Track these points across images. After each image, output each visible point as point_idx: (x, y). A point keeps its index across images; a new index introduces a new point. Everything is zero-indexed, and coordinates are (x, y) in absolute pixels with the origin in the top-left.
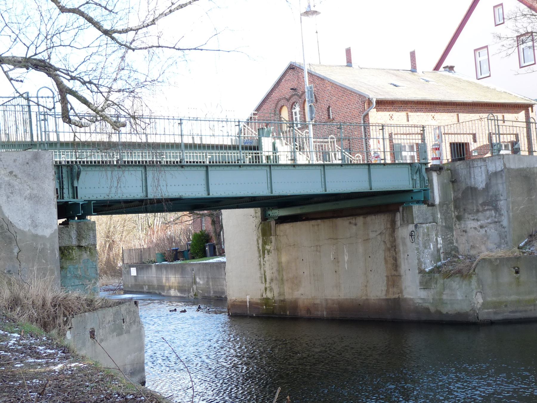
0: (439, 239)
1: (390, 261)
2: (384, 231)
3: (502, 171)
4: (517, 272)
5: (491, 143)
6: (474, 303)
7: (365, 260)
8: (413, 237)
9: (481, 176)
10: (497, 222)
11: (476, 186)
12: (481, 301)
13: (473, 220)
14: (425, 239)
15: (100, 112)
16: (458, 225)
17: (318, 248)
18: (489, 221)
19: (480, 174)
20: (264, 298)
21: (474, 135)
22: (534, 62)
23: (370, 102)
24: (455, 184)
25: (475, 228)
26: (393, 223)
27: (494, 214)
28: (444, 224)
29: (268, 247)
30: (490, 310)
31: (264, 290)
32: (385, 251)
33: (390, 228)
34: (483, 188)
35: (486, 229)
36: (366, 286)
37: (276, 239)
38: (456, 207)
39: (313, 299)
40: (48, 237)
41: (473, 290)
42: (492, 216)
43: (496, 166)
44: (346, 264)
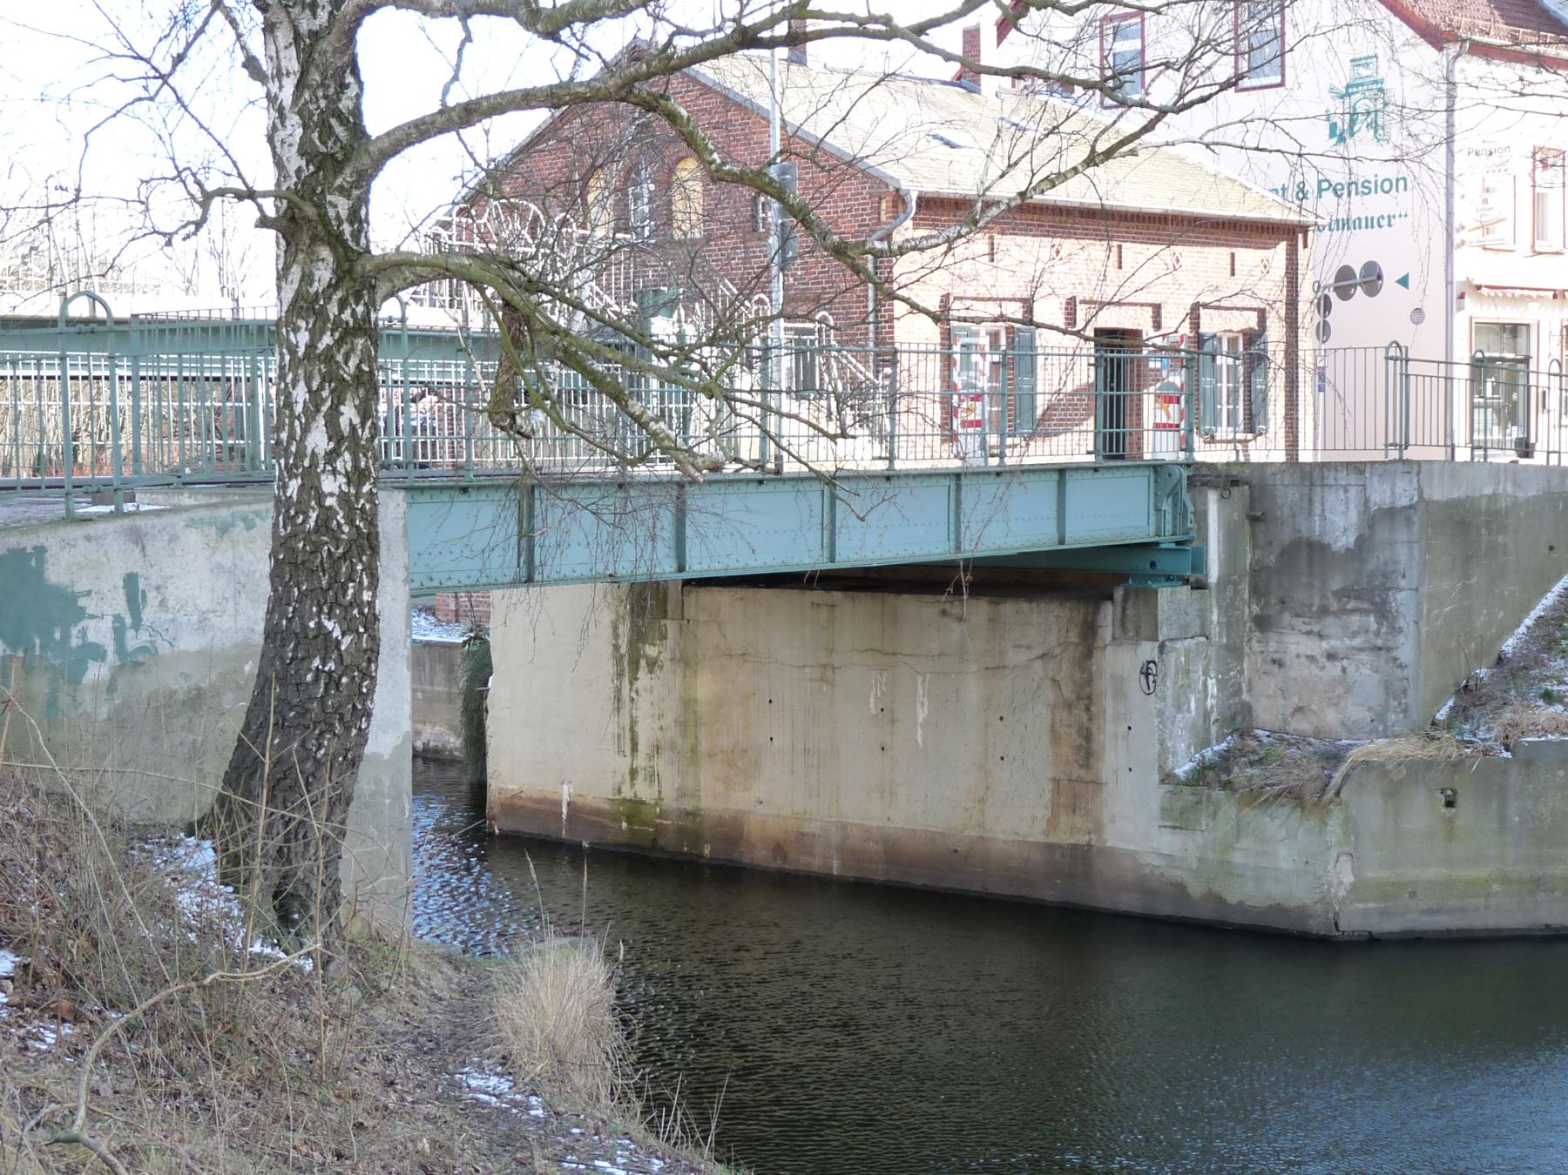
0: (1211, 683)
1: (1071, 737)
2: (1057, 651)
3: (1411, 507)
4: (1450, 804)
5: (1198, 333)
6: (1330, 885)
7: (986, 726)
8: (1151, 678)
9: (1346, 513)
10: (1380, 649)
11: (1327, 540)
12: (1348, 878)
13: (1308, 633)
14: (1180, 683)
15: (652, 424)
16: (1259, 642)
17: (829, 672)
18: (1357, 642)
19: (1342, 508)
20: (624, 800)
21: (1157, 309)
22: (1278, 79)
23: (899, 199)
24: (1260, 527)
25: (1311, 658)
26: (1090, 631)
27: (1374, 626)
28: (1225, 641)
29: (651, 651)
30: (1371, 905)
31: (628, 778)
32: (1054, 708)
33: (1078, 645)
34: (1348, 549)
35: (1345, 663)
36: (982, 801)
37: (681, 629)
38: (1255, 591)
39: (797, 819)
40: (386, 757)
41: (1329, 848)
42: (1367, 631)
43: (1393, 492)
44: (920, 732)
